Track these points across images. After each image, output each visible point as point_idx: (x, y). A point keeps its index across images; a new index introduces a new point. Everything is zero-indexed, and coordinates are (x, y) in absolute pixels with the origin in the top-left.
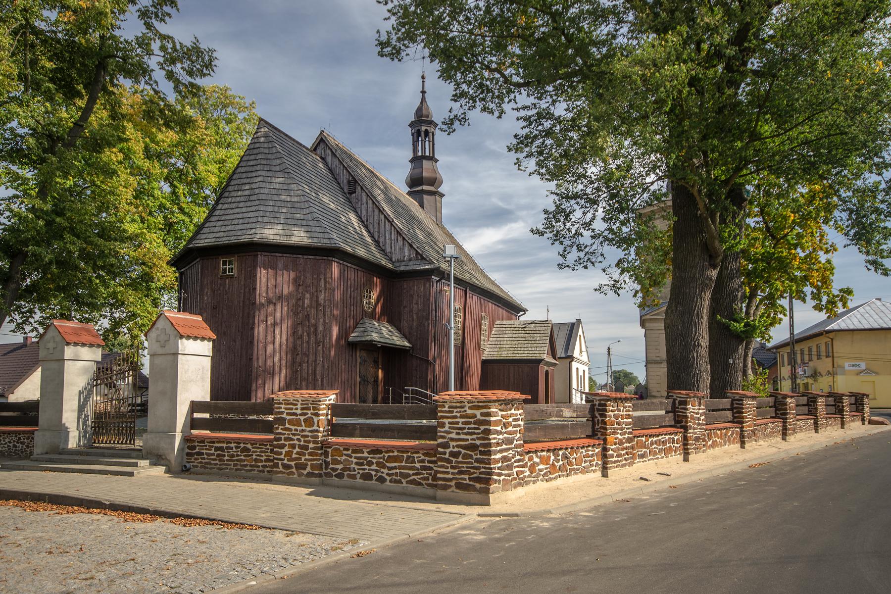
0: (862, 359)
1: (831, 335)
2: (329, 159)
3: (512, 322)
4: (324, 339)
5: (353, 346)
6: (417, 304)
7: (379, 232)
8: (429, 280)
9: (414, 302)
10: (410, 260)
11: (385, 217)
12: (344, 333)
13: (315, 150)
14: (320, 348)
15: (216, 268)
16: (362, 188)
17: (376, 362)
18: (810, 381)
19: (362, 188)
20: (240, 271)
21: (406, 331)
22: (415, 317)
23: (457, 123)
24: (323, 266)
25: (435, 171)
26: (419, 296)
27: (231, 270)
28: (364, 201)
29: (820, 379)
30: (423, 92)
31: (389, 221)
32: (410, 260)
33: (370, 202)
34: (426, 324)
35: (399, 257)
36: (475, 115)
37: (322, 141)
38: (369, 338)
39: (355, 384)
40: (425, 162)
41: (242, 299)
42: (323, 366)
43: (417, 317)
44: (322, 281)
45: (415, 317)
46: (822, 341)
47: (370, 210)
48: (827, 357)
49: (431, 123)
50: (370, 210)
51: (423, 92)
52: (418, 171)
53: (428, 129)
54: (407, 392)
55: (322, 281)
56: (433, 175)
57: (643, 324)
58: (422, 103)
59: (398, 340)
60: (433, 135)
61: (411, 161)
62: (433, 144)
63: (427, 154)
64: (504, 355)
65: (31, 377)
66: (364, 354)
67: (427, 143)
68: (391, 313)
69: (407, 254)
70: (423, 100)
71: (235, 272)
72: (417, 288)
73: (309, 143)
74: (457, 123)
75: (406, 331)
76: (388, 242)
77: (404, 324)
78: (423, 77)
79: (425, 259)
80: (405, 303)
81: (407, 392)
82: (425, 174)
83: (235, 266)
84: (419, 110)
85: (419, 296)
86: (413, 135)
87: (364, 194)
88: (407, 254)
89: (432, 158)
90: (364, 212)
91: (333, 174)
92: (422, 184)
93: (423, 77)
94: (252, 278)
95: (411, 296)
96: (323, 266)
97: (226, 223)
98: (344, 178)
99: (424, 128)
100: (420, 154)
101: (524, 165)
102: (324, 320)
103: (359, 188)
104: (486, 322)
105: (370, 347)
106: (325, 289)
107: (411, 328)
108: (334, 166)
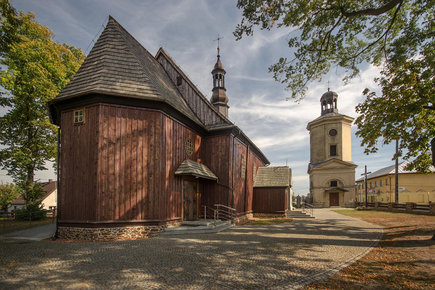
0: (403, 186)
1: (390, 176)
2: (165, 65)
3: (263, 167)
4: (155, 172)
5: (179, 177)
6: (221, 151)
7: (196, 108)
8: (229, 136)
9: (219, 150)
10: (216, 124)
11: (200, 98)
12: (174, 168)
13: (157, 59)
14: (152, 178)
15: (72, 118)
16: (186, 81)
17: (195, 189)
18: (375, 195)
19: (186, 81)
20: (87, 119)
21: (214, 169)
22: (220, 160)
23: (244, 33)
24: (153, 116)
25: (225, 95)
26: (222, 147)
27: (81, 119)
28: (187, 89)
29: (381, 194)
30: (218, 56)
31: (203, 100)
32: (216, 124)
33: (191, 89)
34: (227, 164)
35: (209, 122)
36: (257, 28)
37: (161, 54)
38: (190, 171)
39: (181, 204)
40: (220, 90)
41: (89, 141)
42: (154, 192)
43: (222, 160)
44: (153, 127)
45: (220, 160)
46: (388, 177)
47: (191, 94)
48: (387, 185)
49: (223, 71)
50: (191, 94)
51: (218, 56)
52: (216, 94)
53: (221, 74)
54: (215, 208)
55: (153, 127)
56: (224, 97)
57: (309, 172)
58: (218, 61)
59: (211, 175)
60: (224, 77)
61: (213, 91)
62: (224, 82)
63: (221, 86)
64: (265, 185)
65: (49, 196)
66: (186, 182)
67: (221, 82)
68: (204, 157)
69: (214, 120)
70: (218, 60)
71: (84, 120)
72: (221, 141)
73: (154, 54)
74: (244, 33)
75: (214, 169)
76: (202, 113)
77: (213, 164)
78: (218, 49)
79: (227, 123)
80: (213, 152)
81: (215, 208)
82: (220, 96)
83: (84, 116)
84: (217, 64)
85: (222, 147)
86: (213, 77)
87: (187, 85)
88: (214, 120)
89: (223, 88)
90: (187, 96)
91: (168, 74)
92: (219, 101)
93: (218, 49)
94: (95, 125)
95: (217, 147)
96: (153, 116)
97: (78, 84)
98: (174, 76)
99: (219, 73)
100: (217, 86)
101: (278, 77)
102: (155, 157)
103: (183, 82)
104: (255, 167)
105: (190, 177)
106: (155, 134)
107: (218, 167)
108: (168, 69)
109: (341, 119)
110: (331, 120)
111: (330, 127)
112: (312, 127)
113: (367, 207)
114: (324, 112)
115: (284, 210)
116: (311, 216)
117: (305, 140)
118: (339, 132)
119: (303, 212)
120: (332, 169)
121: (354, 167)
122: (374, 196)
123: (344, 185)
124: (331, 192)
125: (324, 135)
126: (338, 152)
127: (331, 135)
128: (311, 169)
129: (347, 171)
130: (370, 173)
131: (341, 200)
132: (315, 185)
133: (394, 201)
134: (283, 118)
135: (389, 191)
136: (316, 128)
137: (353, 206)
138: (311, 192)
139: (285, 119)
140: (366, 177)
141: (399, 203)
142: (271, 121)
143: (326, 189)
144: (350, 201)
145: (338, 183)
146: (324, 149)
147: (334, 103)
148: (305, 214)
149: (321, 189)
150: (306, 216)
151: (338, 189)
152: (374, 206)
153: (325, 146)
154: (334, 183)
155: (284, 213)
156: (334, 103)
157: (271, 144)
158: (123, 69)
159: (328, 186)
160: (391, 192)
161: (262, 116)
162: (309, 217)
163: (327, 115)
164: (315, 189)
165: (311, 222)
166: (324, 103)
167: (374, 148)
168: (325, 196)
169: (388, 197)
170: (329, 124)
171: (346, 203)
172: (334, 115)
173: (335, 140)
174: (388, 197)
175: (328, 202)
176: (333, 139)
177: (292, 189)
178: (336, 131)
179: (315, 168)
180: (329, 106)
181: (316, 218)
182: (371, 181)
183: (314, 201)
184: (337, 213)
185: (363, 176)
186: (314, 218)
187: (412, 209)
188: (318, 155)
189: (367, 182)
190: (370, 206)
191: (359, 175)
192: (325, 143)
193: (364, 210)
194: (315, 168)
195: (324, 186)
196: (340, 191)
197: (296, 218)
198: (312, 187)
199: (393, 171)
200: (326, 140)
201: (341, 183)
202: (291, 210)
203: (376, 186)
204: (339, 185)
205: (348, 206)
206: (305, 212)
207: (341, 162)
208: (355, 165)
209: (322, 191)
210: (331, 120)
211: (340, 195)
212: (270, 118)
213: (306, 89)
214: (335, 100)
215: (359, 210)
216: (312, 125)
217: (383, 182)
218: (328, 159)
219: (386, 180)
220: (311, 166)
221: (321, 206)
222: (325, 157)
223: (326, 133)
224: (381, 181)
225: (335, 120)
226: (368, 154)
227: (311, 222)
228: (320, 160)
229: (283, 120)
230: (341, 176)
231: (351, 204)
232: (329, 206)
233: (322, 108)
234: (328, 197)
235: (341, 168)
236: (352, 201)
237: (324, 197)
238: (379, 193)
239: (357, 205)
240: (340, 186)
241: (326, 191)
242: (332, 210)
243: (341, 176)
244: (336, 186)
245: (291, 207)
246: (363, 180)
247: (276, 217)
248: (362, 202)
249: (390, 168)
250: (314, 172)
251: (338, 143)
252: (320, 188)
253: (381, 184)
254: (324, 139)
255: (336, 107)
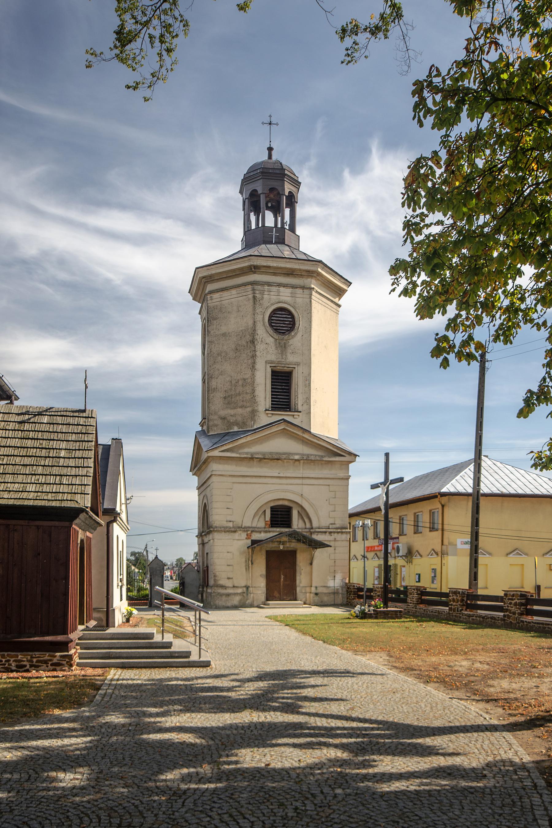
1: (444, 499)
29: (417, 560)
46: (435, 505)
48: (432, 529)
57: (198, 464)
109: (311, 274)
110: (276, 272)
111: (274, 298)
112: (210, 287)
113: (386, 605)
114: (252, 238)
115: (65, 632)
116: (194, 657)
117: (186, 364)
118: (301, 324)
119: (158, 638)
120: (275, 459)
121: (348, 458)
122: (396, 565)
123: (315, 524)
124: (272, 546)
125: (250, 323)
126: (298, 399)
127: (276, 330)
128: (204, 456)
129: (326, 472)
130: (401, 480)
131: (302, 580)
132: (218, 517)
133: (464, 584)
134: (110, 275)
135: (438, 548)
136: (225, 294)
137: (339, 599)
138: (202, 544)
139: (117, 279)
140: (387, 494)
141: (480, 592)
142: (63, 276)
143: (256, 536)
144: (331, 584)
145: (295, 513)
146: (251, 383)
147: (287, 211)
148: (169, 645)
149: (236, 536)
150: (172, 655)
151: (298, 537)
152: (404, 601)
153: (253, 367)
154: (280, 515)
155: (64, 646)
156: (287, 211)
157: (66, 364)
158: (40, 437)
159: (262, 524)
160: (443, 554)
161: (30, 251)
162: (182, 660)
163: (263, 249)
164: (216, 535)
165: (193, 699)
166: (253, 204)
167: (471, 338)
168: (250, 562)
169: (434, 570)
170: (269, 284)
171: (320, 590)
172: (287, 253)
173: (289, 351)
174: (434, 570)
175: (262, 583)
176: (283, 347)
177: (125, 529)
178: (293, 317)
179: (216, 453)
180: (270, 220)
181: (217, 666)
182: (402, 511)
183: (211, 582)
184: (293, 634)
185: (379, 491)
186: (206, 665)
187: (521, 614)
188: (229, 401)
189: (394, 515)
190: (386, 599)
191: (361, 490)
192: (254, 357)
193: (377, 615)
194: (216, 453)
195: (247, 523)
196: (299, 546)
197: (123, 667)
198: (206, 528)
199: (463, 483)
200: (260, 347)
201: (304, 514)
202: (118, 618)
203: (402, 533)
204: (297, 524)
205: (325, 599)
206: (168, 637)
207: (303, 434)
208: (350, 454)
209: (240, 542)
210: (276, 272)
211: (301, 560)
212: (62, 262)
213: (177, 27)
214: (292, 201)
215: (363, 616)
216: (209, 279)
217: (425, 518)
218: (264, 419)
219: (432, 513)
220: (205, 443)
221: (236, 600)
222: (254, 413)
223: (259, 318)
224: (416, 517)
225: (290, 273)
226: (445, 364)
227: (193, 699)
228: (236, 424)
229: (108, 281)
230: (307, 490)
231: (335, 593)
232: (263, 598)
233: (247, 221)
234: (260, 568)
235: (307, 460)
236: (336, 583)
237: (247, 568)
238: (410, 554)
239: (352, 595)
240: (301, 525)
241: (254, 542)
242: (275, 618)
243: (307, 490)
244: (289, 525)
245: (120, 605)
246: (378, 509)
247: (20, 668)
248: (369, 585)
249: (457, 469)
250: (215, 467)
251: (298, 364)
252: (233, 530)
253: (416, 526)
254: (253, 342)
255: (292, 229)
